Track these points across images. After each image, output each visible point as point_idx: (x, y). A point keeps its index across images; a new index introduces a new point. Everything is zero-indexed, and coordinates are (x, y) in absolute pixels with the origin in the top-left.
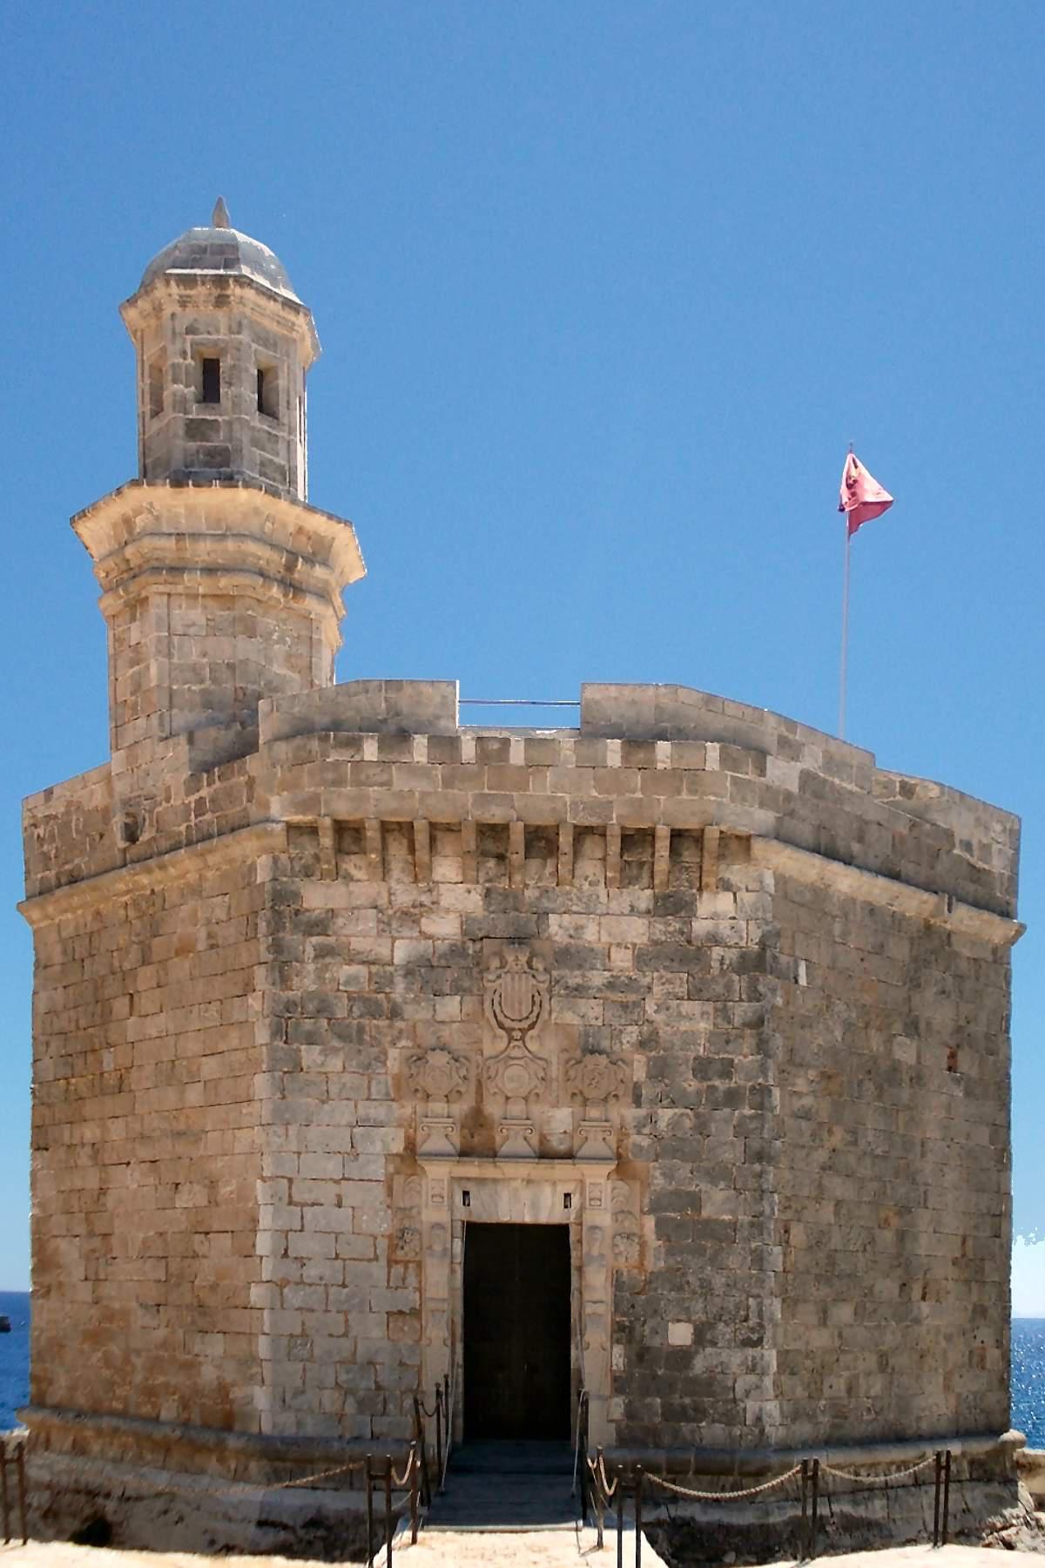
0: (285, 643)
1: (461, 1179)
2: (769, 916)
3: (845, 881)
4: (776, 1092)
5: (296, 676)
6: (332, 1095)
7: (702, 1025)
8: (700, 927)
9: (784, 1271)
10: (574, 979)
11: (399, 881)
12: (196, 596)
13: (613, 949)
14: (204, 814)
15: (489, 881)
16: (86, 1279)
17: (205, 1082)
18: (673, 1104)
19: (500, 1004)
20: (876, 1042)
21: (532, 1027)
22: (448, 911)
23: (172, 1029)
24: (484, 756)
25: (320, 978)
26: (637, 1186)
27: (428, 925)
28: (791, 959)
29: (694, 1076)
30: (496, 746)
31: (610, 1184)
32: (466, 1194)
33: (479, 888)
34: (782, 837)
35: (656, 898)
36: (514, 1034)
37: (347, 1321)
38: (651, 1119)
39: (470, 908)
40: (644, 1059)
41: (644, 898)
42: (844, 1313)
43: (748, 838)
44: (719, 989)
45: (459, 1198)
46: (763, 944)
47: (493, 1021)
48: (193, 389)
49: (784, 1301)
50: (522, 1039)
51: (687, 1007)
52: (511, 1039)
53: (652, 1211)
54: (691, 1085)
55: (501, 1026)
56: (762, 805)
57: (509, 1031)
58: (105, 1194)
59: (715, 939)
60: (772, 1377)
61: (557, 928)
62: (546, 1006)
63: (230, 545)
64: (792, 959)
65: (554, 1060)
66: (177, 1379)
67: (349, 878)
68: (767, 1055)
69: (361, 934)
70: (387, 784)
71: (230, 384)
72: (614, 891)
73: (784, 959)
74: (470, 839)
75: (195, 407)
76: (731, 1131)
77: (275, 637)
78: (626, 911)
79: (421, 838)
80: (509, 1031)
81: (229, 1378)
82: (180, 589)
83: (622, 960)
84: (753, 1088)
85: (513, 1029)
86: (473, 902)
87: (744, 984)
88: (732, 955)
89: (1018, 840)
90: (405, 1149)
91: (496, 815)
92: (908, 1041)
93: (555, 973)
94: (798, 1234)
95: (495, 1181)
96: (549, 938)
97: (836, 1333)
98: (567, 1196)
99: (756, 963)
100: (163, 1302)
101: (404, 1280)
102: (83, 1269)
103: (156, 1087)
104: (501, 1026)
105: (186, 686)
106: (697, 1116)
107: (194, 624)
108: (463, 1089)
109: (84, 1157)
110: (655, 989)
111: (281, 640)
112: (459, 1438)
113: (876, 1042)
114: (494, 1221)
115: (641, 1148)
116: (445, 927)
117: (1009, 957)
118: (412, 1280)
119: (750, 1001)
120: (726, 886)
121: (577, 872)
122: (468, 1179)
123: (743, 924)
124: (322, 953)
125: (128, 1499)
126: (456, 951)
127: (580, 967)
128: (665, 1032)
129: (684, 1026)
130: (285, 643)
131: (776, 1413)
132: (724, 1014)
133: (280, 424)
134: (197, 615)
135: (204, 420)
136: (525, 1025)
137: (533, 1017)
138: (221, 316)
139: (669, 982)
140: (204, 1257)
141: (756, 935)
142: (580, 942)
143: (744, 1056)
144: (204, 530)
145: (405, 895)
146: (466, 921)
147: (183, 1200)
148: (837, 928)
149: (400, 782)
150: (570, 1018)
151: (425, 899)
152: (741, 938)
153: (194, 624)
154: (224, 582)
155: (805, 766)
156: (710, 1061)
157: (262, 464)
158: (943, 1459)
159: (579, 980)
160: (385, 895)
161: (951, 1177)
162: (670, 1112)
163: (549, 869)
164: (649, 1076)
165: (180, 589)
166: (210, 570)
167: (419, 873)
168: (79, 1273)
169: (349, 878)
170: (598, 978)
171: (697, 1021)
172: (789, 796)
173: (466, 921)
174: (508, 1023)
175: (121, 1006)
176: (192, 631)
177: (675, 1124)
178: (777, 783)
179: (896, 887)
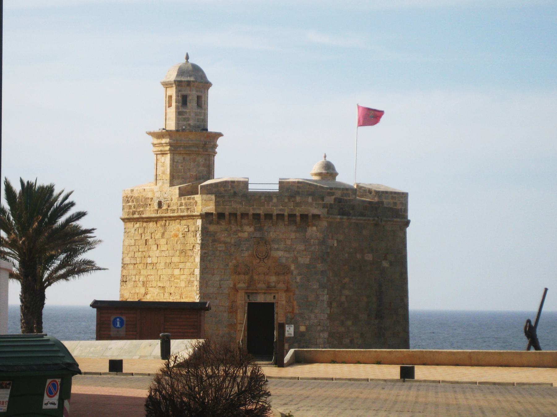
6: (215, 273)
11: (233, 225)
14: (182, 206)
17: (180, 269)
19: (258, 252)
20: (359, 256)
21: (266, 257)
36: (261, 259)
42: (349, 323)
47: (256, 257)
50: (263, 260)
52: (260, 260)
55: (258, 257)
57: (260, 258)
67: (221, 224)
71: (190, 103)
74: (251, 217)
80: (260, 258)
85: (261, 258)
86: (251, 229)
91: (258, 212)
95: (256, 293)
103: (165, 269)
105: (177, 174)
109: (140, 284)
113: (359, 256)
135: (183, 111)
136: (264, 257)
137: (266, 256)
145: (234, 228)
151: (239, 229)
157: (198, 119)
169: (221, 224)
172: (331, 204)
174: (259, 257)
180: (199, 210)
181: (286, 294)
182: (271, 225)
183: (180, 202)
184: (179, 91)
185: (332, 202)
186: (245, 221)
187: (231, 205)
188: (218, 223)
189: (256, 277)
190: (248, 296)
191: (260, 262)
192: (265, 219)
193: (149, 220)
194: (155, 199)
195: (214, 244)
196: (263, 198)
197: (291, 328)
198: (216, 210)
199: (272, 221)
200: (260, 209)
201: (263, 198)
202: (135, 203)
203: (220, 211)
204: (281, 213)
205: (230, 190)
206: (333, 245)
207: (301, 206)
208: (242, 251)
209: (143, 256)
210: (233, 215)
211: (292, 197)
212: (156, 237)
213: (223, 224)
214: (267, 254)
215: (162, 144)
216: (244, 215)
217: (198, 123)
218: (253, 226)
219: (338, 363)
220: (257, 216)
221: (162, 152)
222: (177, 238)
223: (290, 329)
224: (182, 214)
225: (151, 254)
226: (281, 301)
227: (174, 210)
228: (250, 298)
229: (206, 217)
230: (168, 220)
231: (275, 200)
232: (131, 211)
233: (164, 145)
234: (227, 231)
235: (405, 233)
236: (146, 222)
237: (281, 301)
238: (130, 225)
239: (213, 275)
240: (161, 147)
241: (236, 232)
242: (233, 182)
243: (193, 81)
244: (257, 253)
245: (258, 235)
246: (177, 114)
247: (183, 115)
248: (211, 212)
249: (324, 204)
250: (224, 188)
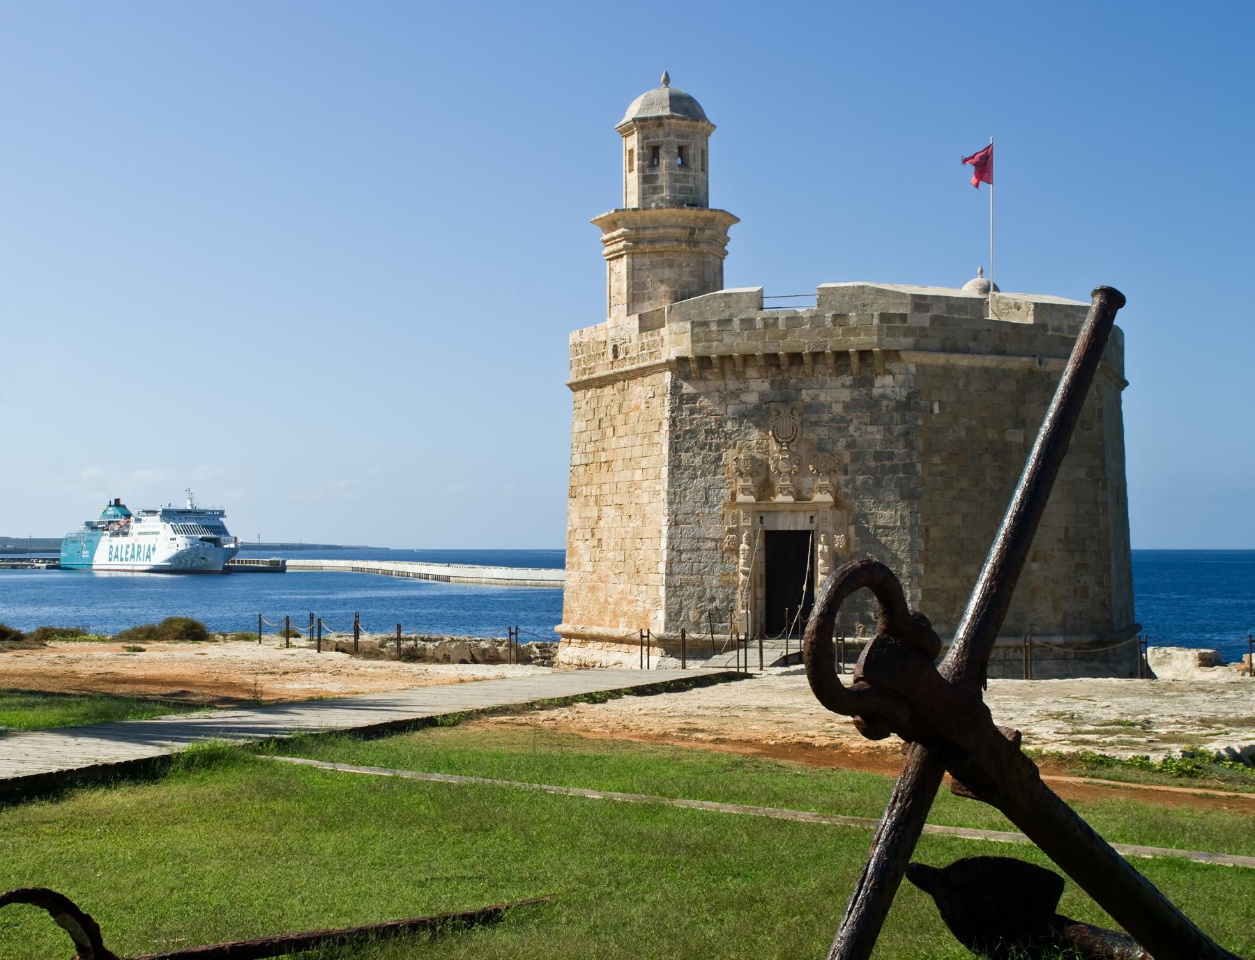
0: (690, 266)
1: (758, 511)
2: (912, 385)
3: (962, 361)
4: (919, 466)
7: (878, 436)
8: (876, 392)
9: (926, 550)
10: (814, 418)
11: (730, 379)
12: (646, 253)
13: (833, 404)
15: (773, 376)
18: (863, 473)
21: (792, 441)
22: (753, 391)
23: (630, 444)
24: (766, 326)
26: (845, 512)
27: (744, 398)
28: (928, 403)
29: (874, 459)
31: (832, 512)
32: (762, 518)
33: (768, 380)
34: (917, 348)
35: (854, 380)
38: (853, 481)
39: (764, 389)
40: (849, 454)
41: (848, 380)
43: (899, 351)
44: (886, 420)
45: (758, 520)
46: (909, 397)
48: (647, 162)
49: (926, 565)
51: (870, 428)
53: (853, 523)
54: (873, 464)
56: (905, 336)
59: (883, 396)
61: (805, 395)
62: (800, 432)
63: (661, 231)
64: (928, 403)
65: (804, 455)
67: (706, 379)
68: (912, 448)
70: (721, 340)
72: (834, 378)
73: (923, 403)
75: (647, 170)
76: (893, 484)
77: (684, 265)
78: (840, 386)
79: (739, 362)
82: (638, 250)
83: (838, 409)
84: (904, 465)
86: (766, 386)
87: (899, 417)
88: (892, 404)
92: (1017, 431)
93: (805, 416)
95: (775, 511)
96: (802, 400)
98: (812, 517)
99: (905, 406)
106: (876, 478)
107: (644, 264)
108: (759, 471)
110: (854, 420)
113: (991, 434)
114: (775, 529)
115: (847, 494)
116: (752, 398)
119: (902, 424)
120: (890, 372)
121: (816, 370)
122: (762, 511)
123: (898, 389)
126: (757, 408)
127: (817, 412)
128: (859, 440)
129: (869, 437)
130: (690, 266)
132: (889, 430)
133: (690, 170)
134: (646, 260)
136: (789, 440)
137: (793, 437)
138: (661, 131)
139: (861, 417)
141: (904, 393)
142: (817, 402)
143: (900, 449)
144: (649, 225)
145: (732, 385)
146: (762, 394)
148: (961, 383)
149: (727, 339)
150: (812, 436)
151: (742, 386)
152: (897, 395)
153: (644, 264)
154: (658, 246)
155: (935, 313)
156: (882, 452)
159: (816, 419)
160: (723, 385)
161: (17, 610)
162: (862, 477)
163: (801, 370)
164: (852, 461)
165: (638, 250)
166: (652, 241)
167: (740, 376)
168: (587, 557)
170: (826, 417)
171: (875, 434)
172: (923, 329)
173: (762, 394)
175: (609, 431)
176: (643, 268)
177: (865, 482)
178: (914, 325)
179: (1000, 358)
180: (670, 352)
181: (834, 513)
184: (645, 138)
185: (927, 324)
188: (702, 378)
193: (602, 382)
194: (609, 342)
198: (693, 351)
202: (585, 355)
203: (700, 351)
209: (596, 449)
210: (725, 359)
213: (710, 377)
214: (794, 433)
216: (747, 358)
217: (681, 196)
218: (768, 380)
222: (638, 412)
224: (642, 365)
225: (606, 444)
228: (764, 522)
229: (679, 366)
232: (581, 369)
235: (1118, 402)
236: (601, 387)
238: (580, 394)
243: (667, 117)
246: (641, 181)
248: (686, 355)
249: (908, 328)
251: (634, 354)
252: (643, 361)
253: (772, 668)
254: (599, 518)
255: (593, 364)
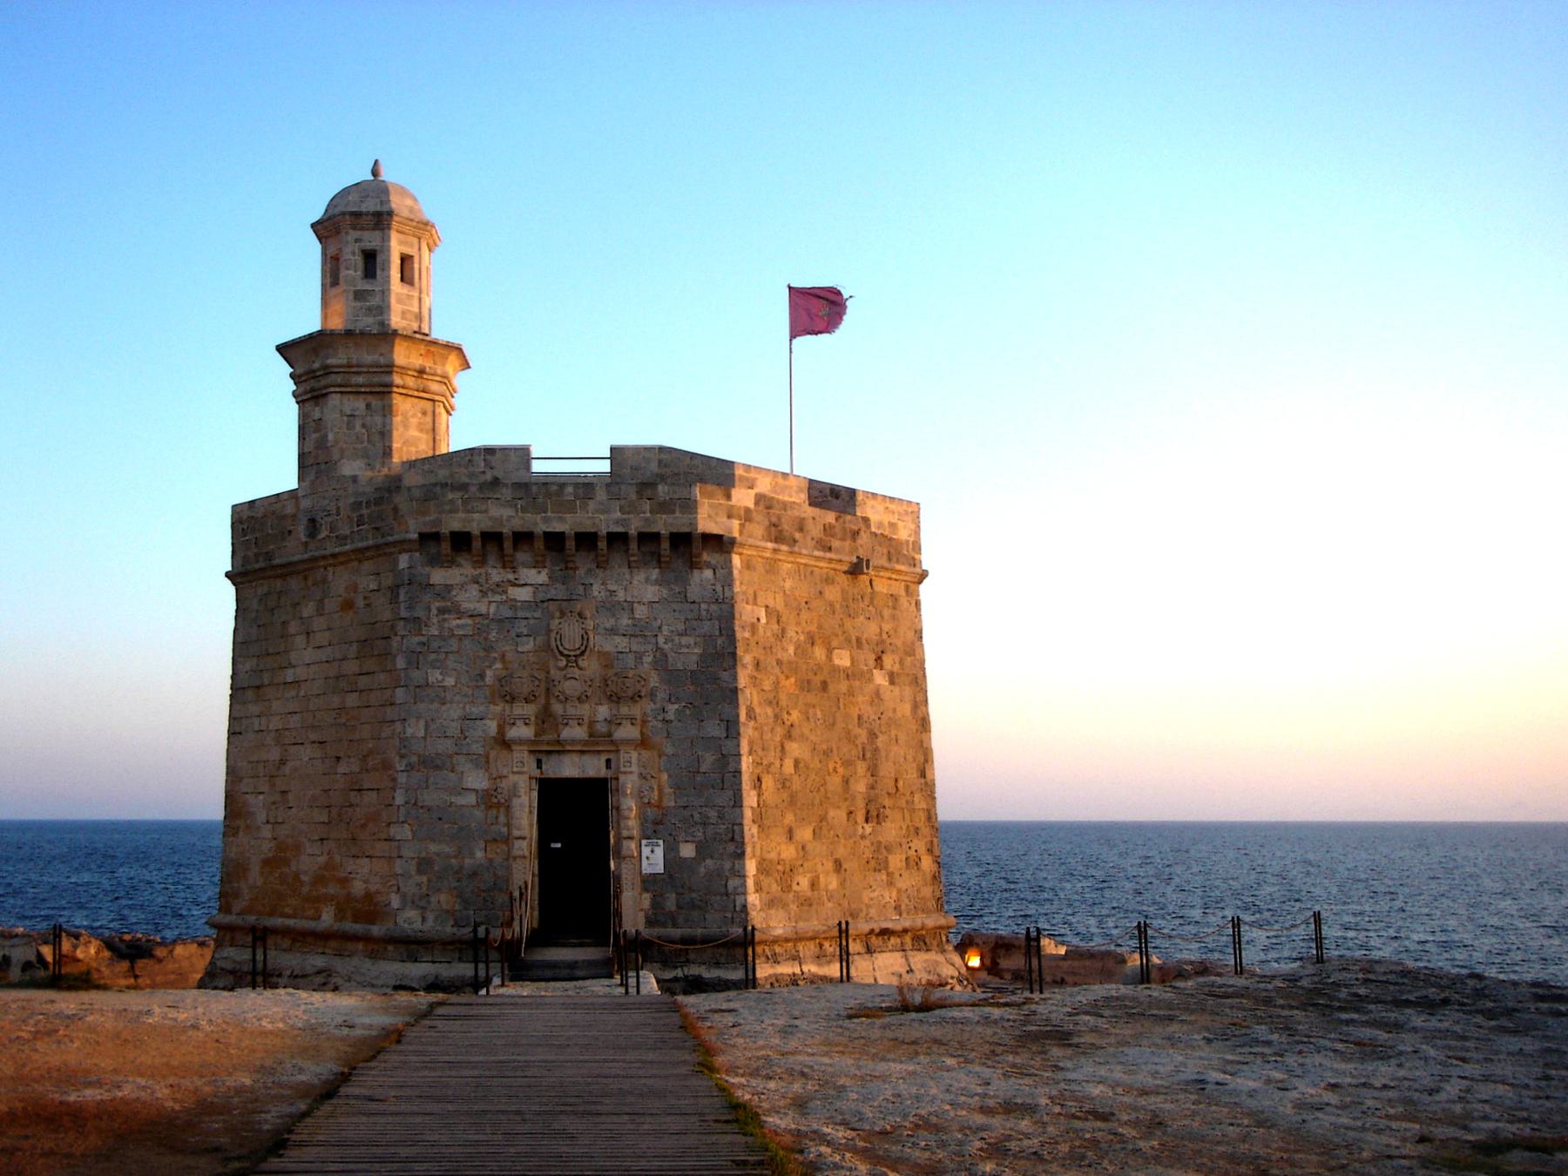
5: (424, 436)
16: (268, 822)
20: (819, 653)
23: (339, 656)
25: (441, 628)
30: (555, 488)
37: (320, 631)
42: (805, 834)
47: (556, 651)
50: (576, 661)
51: (684, 640)
52: (568, 661)
58: (284, 764)
60: (752, 878)
66: (332, 889)
69: (470, 599)
81: (373, 888)
85: (569, 656)
89: (918, 517)
90: (498, 733)
91: (557, 527)
94: (768, 782)
95: (558, 752)
97: (800, 847)
100: (326, 837)
101: (497, 818)
102: (264, 815)
104: (561, 653)
111: (414, 416)
112: (535, 925)
114: (558, 776)
117: (918, 592)
118: (502, 819)
124: (442, 611)
125: (296, 977)
131: (757, 902)
136: (578, 652)
137: (583, 648)
140: (357, 805)
145: (496, 575)
147: (342, 768)
158: (844, 926)
174: (566, 652)
182: (594, 566)
183: (358, 514)
186: (522, 556)
187: (486, 511)
189: (557, 708)
190: (539, 762)
191: (567, 665)
192: (577, 550)
195: (444, 620)
196: (570, 489)
197: (656, 849)
199: (597, 556)
200: (561, 520)
201: (570, 489)
204: (620, 529)
205: (484, 472)
206: (758, 619)
207: (673, 512)
208: (518, 636)
210: (492, 538)
211: (646, 487)
212: (305, 614)
214: (585, 643)
215: (314, 371)
216: (523, 538)
219: (287, 362)
220: (555, 541)
221: (316, 394)
223: (652, 851)
226: (625, 773)
227: (345, 538)
228: (544, 767)
230: (330, 565)
231: (601, 495)
233: (318, 374)
234: (478, 583)
236: (283, 576)
237: (625, 773)
239: (444, 704)
240: (312, 381)
241: (500, 587)
242: (489, 451)
244: (559, 643)
245: (558, 591)
247: (365, 300)
250: (467, 468)
251: (345, 530)
252: (362, 540)
253: (35, 953)
254: (283, 762)
255: (272, 547)
